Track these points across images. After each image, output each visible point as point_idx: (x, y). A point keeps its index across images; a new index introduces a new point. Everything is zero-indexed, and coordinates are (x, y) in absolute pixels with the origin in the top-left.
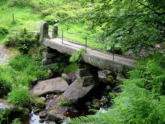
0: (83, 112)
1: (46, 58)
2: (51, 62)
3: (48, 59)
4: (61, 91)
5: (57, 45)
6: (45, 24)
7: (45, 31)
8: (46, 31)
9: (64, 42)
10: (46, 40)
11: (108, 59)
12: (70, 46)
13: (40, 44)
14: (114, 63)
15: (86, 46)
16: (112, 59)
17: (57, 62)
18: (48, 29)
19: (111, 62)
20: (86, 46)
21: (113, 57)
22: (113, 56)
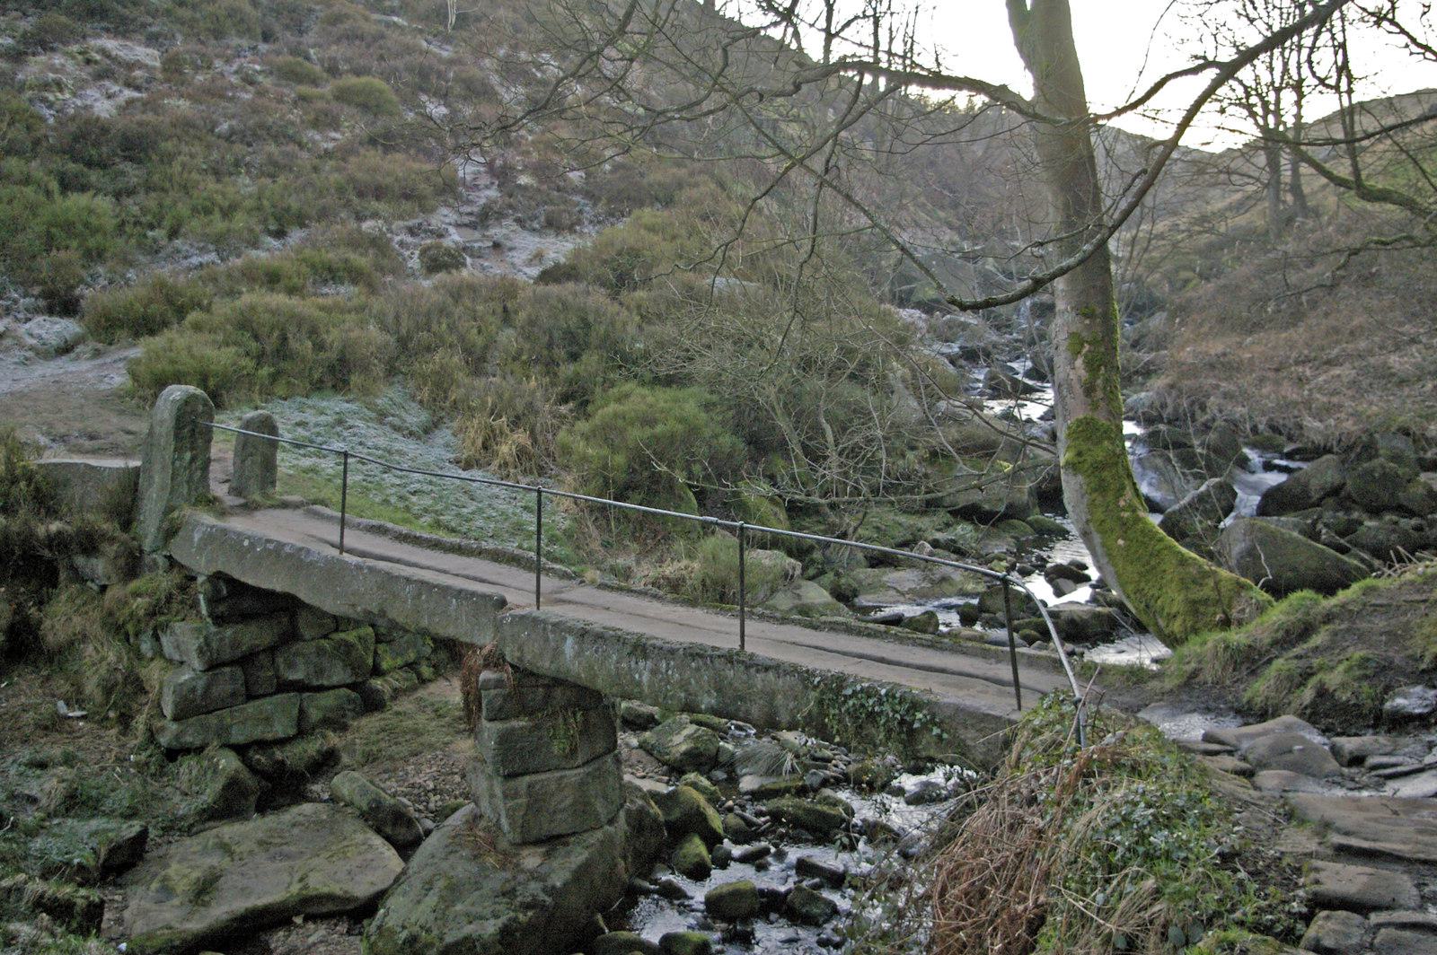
0: (829, 125)
1: (197, 664)
2: (233, 694)
3: (213, 666)
4: (349, 900)
5: (295, 560)
6: (186, 403)
7: (188, 456)
8: (193, 460)
9: (352, 539)
10: (198, 524)
11: (709, 641)
12: (398, 561)
13: (147, 560)
14: (753, 665)
15: (341, 548)
16: (730, 643)
17: (285, 687)
18: (209, 441)
19: (729, 658)
20: (341, 548)
21: (738, 630)
22: (737, 622)
